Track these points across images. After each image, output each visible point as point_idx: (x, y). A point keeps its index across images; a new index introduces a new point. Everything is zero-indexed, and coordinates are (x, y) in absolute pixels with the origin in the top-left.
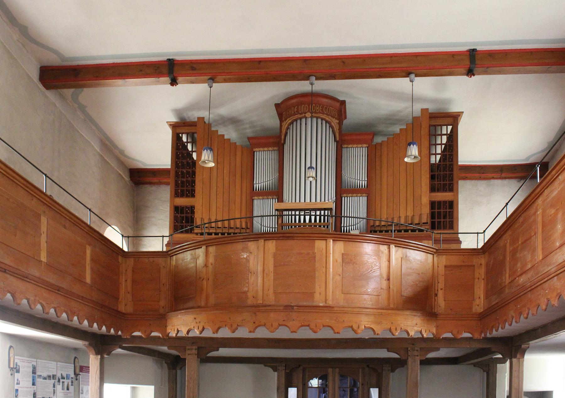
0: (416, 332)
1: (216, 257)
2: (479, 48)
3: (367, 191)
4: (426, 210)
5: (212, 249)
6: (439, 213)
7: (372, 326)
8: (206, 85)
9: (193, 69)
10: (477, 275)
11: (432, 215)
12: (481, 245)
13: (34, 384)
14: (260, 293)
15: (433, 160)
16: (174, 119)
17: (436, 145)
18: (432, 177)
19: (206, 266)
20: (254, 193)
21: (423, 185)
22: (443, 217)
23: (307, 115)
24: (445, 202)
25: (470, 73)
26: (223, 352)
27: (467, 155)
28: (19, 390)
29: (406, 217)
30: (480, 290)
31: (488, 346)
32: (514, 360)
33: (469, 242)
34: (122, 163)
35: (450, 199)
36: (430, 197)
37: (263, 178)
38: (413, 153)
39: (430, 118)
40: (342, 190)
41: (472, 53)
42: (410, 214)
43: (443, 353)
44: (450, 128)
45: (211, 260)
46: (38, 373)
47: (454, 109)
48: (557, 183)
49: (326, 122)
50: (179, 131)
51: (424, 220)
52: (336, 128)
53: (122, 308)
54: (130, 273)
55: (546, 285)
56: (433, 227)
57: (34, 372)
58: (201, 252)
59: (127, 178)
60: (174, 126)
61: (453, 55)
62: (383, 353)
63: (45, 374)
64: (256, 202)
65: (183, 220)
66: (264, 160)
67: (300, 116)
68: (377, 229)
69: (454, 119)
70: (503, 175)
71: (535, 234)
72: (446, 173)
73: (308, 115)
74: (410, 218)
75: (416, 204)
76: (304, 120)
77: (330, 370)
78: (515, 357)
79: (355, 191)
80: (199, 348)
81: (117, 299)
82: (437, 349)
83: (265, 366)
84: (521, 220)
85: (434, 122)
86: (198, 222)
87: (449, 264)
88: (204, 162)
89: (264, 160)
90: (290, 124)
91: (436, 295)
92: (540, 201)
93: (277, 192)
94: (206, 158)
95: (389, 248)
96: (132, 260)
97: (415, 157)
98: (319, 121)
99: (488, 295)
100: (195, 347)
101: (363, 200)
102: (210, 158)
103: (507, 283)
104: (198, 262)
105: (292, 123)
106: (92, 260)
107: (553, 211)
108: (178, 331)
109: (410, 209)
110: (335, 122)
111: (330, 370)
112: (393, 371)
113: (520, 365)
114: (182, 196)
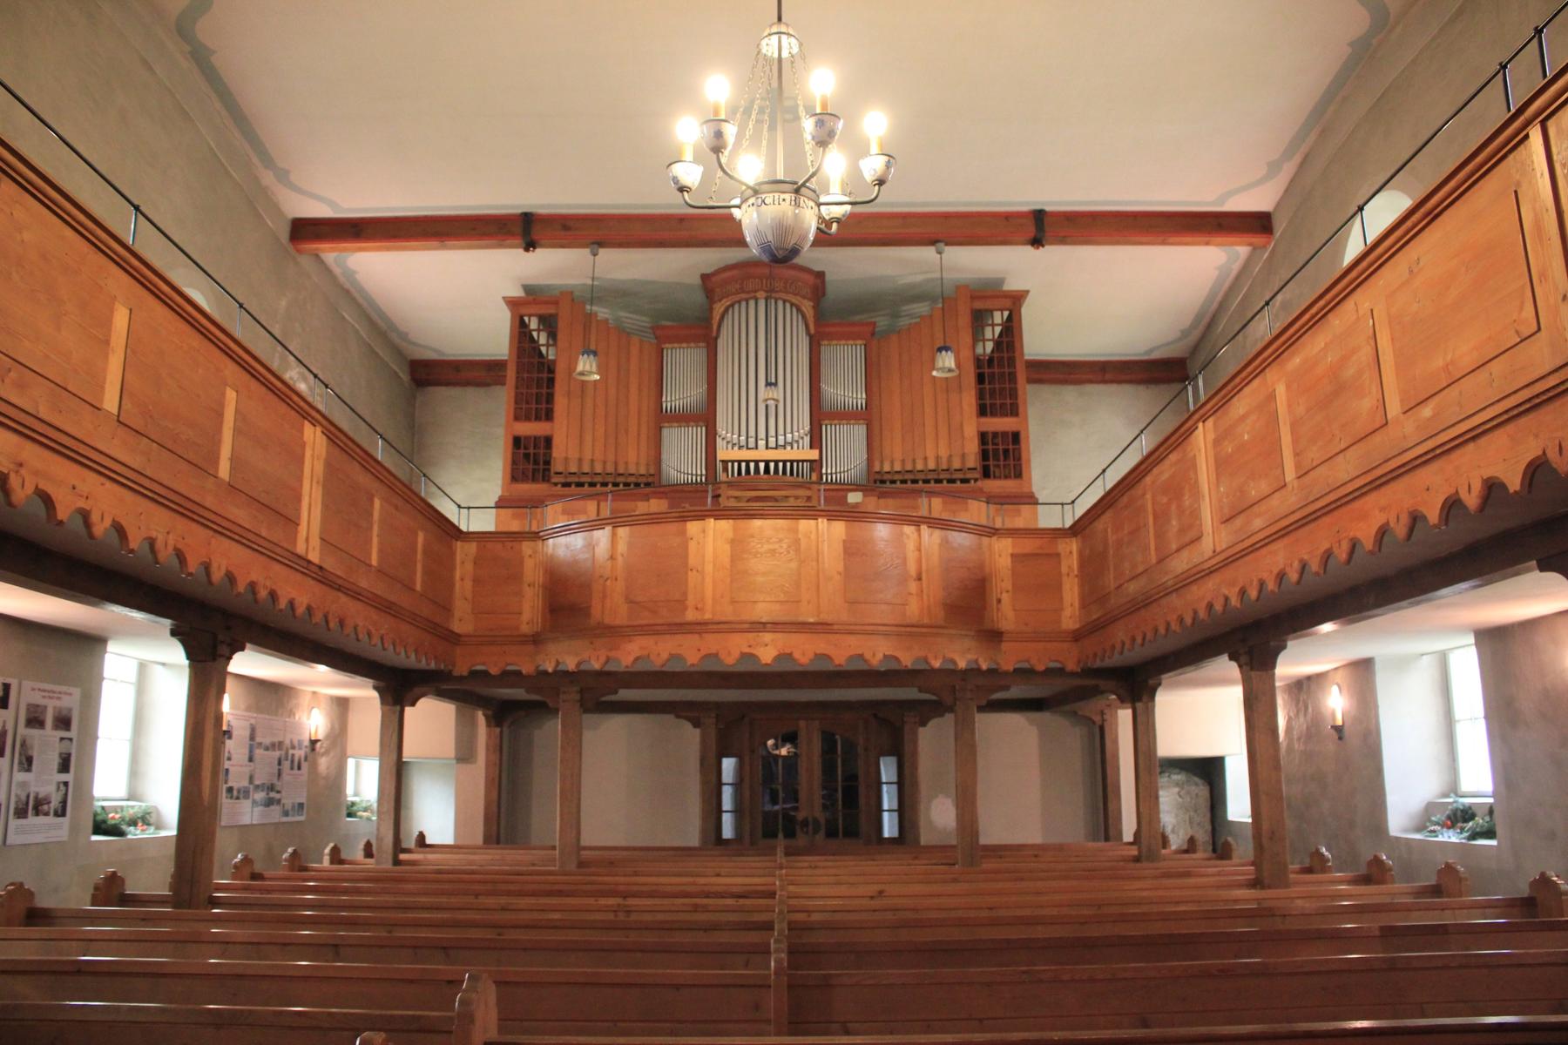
0: (969, 662)
1: (630, 545)
2: (1048, 209)
3: (867, 416)
4: (972, 447)
5: (623, 532)
6: (996, 451)
7: (897, 654)
8: (586, 251)
9: (566, 228)
10: (1064, 569)
11: (984, 455)
12: (1068, 524)
13: (251, 760)
14: (709, 602)
15: (979, 350)
16: (518, 293)
17: (984, 340)
18: (980, 379)
19: (612, 558)
20: (663, 418)
21: (965, 407)
22: (1002, 456)
23: (758, 295)
24: (1005, 434)
25: (1037, 242)
26: (625, 694)
27: (1038, 342)
28: (232, 770)
29: (938, 458)
30: (1071, 593)
31: (1094, 682)
32: (1139, 705)
33: (1049, 518)
34: (398, 352)
35: (1015, 429)
36: (978, 425)
37: (682, 391)
38: (947, 364)
39: (973, 298)
40: (820, 415)
41: (1039, 216)
42: (944, 453)
43: (1015, 692)
44: (1006, 314)
45: (622, 547)
46: (258, 739)
47: (1012, 285)
48: (1167, 462)
49: (792, 305)
50: (523, 311)
51: (971, 464)
52: (810, 313)
53: (457, 627)
54: (469, 566)
55: (1164, 602)
56: (986, 474)
57: (252, 738)
58: (602, 536)
59: (405, 377)
60: (512, 303)
61: (1008, 217)
62: (910, 693)
63: (267, 741)
64: (665, 432)
65: (531, 462)
66: (683, 366)
67: (744, 296)
68: (887, 477)
69: (1016, 300)
70: (1108, 377)
71: (1134, 532)
72: (1003, 376)
73: (761, 294)
74: (944, 460)
75: (954, 437)
76: (752, 303)
77: (802, 723)
78: (1140, 700)
79: (845, 416)
80: (581, 691)
81: (447, 609)
82: (1007, 688)
83: (678, 717)
84: (1125, 499)
85: (979, 305)
86: (557, 466)
87: (1018, 551)
88: (582, 374)
89: (683, 366)
90: (726, 310)
91: (999, 601)
92: (1148, 479)
93: (706, 417)
94: (588, 368)
95: (919, 531)
96: (474, 545)
97: (950, 370)
98: (780, 303)
99: (1084, 605)
100: (576, 688)
101: (859, 431)
102: (594, 369)
103: (1113, 587)
104: (597, 550)
105: (732, 305)
106: (425, 552)
107: (1165, 500)
108: (558, 663)
109: (943, 443)
110: (807, 306)
111: (802, 723)
112: (924, 724)
113: (1150, 713)
114: (528, 419)
